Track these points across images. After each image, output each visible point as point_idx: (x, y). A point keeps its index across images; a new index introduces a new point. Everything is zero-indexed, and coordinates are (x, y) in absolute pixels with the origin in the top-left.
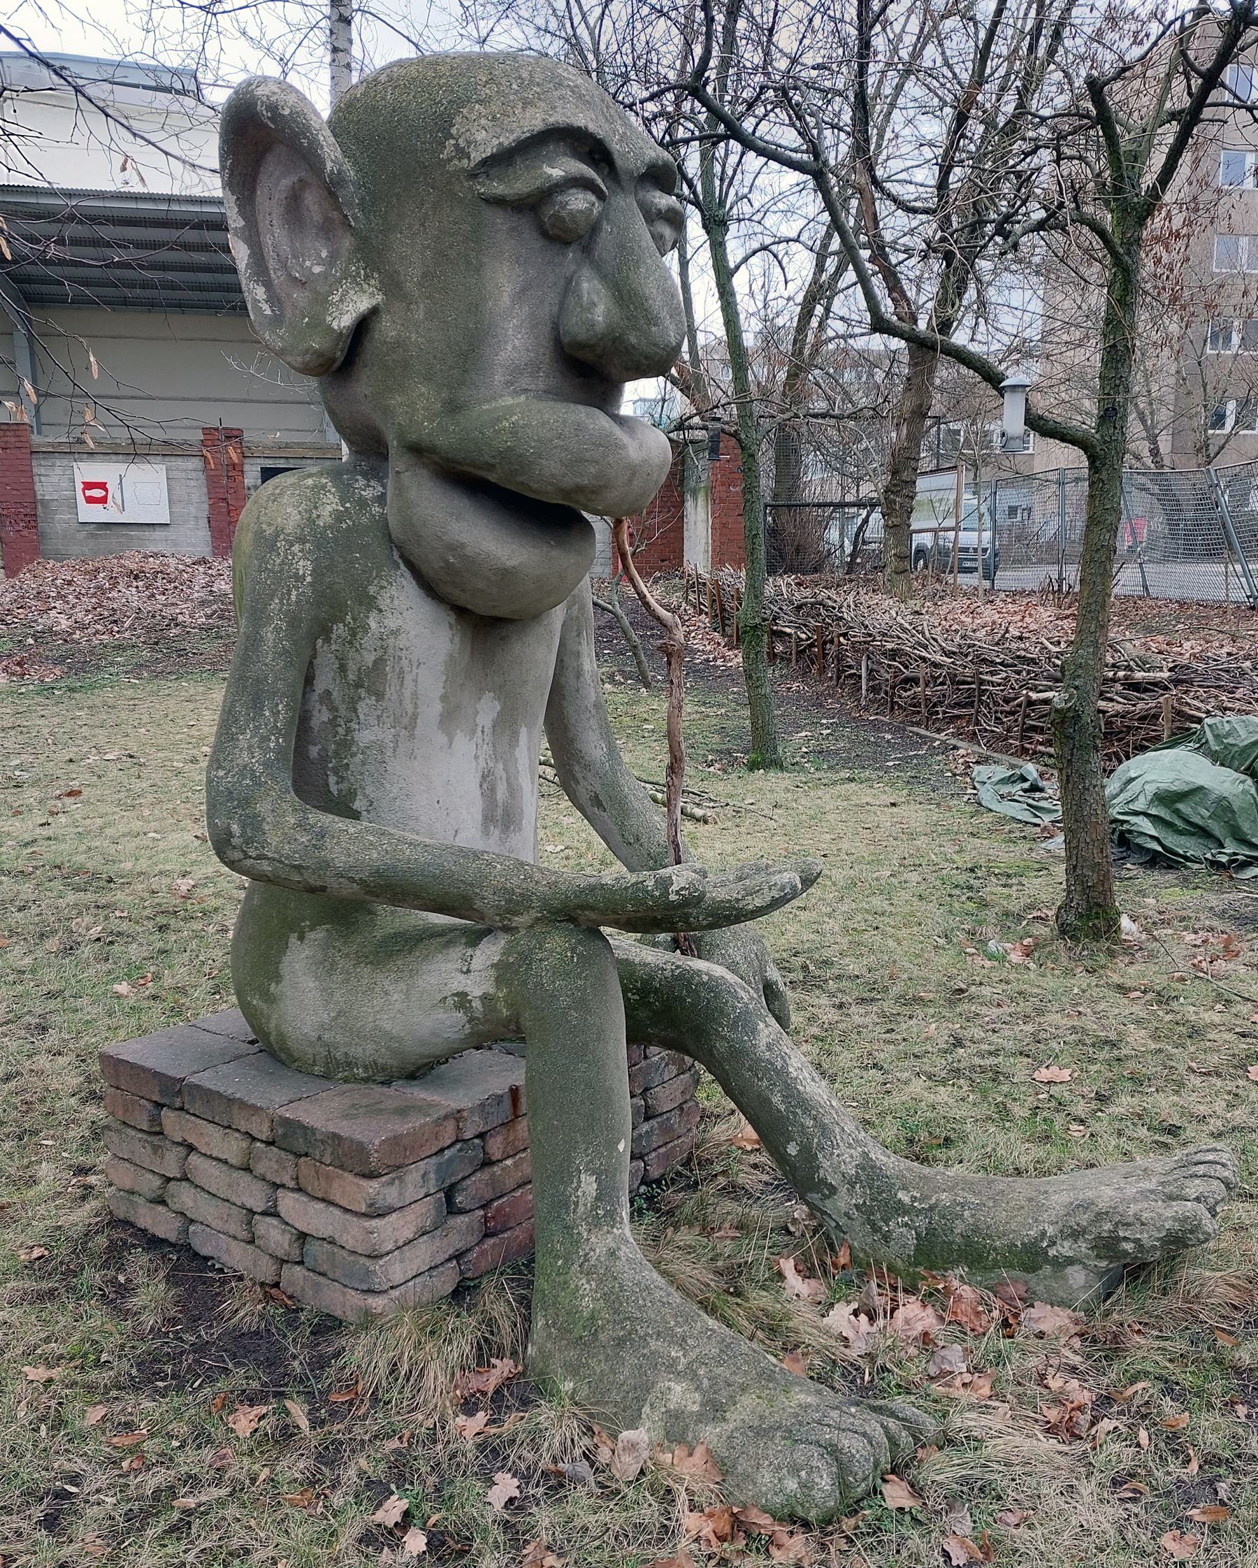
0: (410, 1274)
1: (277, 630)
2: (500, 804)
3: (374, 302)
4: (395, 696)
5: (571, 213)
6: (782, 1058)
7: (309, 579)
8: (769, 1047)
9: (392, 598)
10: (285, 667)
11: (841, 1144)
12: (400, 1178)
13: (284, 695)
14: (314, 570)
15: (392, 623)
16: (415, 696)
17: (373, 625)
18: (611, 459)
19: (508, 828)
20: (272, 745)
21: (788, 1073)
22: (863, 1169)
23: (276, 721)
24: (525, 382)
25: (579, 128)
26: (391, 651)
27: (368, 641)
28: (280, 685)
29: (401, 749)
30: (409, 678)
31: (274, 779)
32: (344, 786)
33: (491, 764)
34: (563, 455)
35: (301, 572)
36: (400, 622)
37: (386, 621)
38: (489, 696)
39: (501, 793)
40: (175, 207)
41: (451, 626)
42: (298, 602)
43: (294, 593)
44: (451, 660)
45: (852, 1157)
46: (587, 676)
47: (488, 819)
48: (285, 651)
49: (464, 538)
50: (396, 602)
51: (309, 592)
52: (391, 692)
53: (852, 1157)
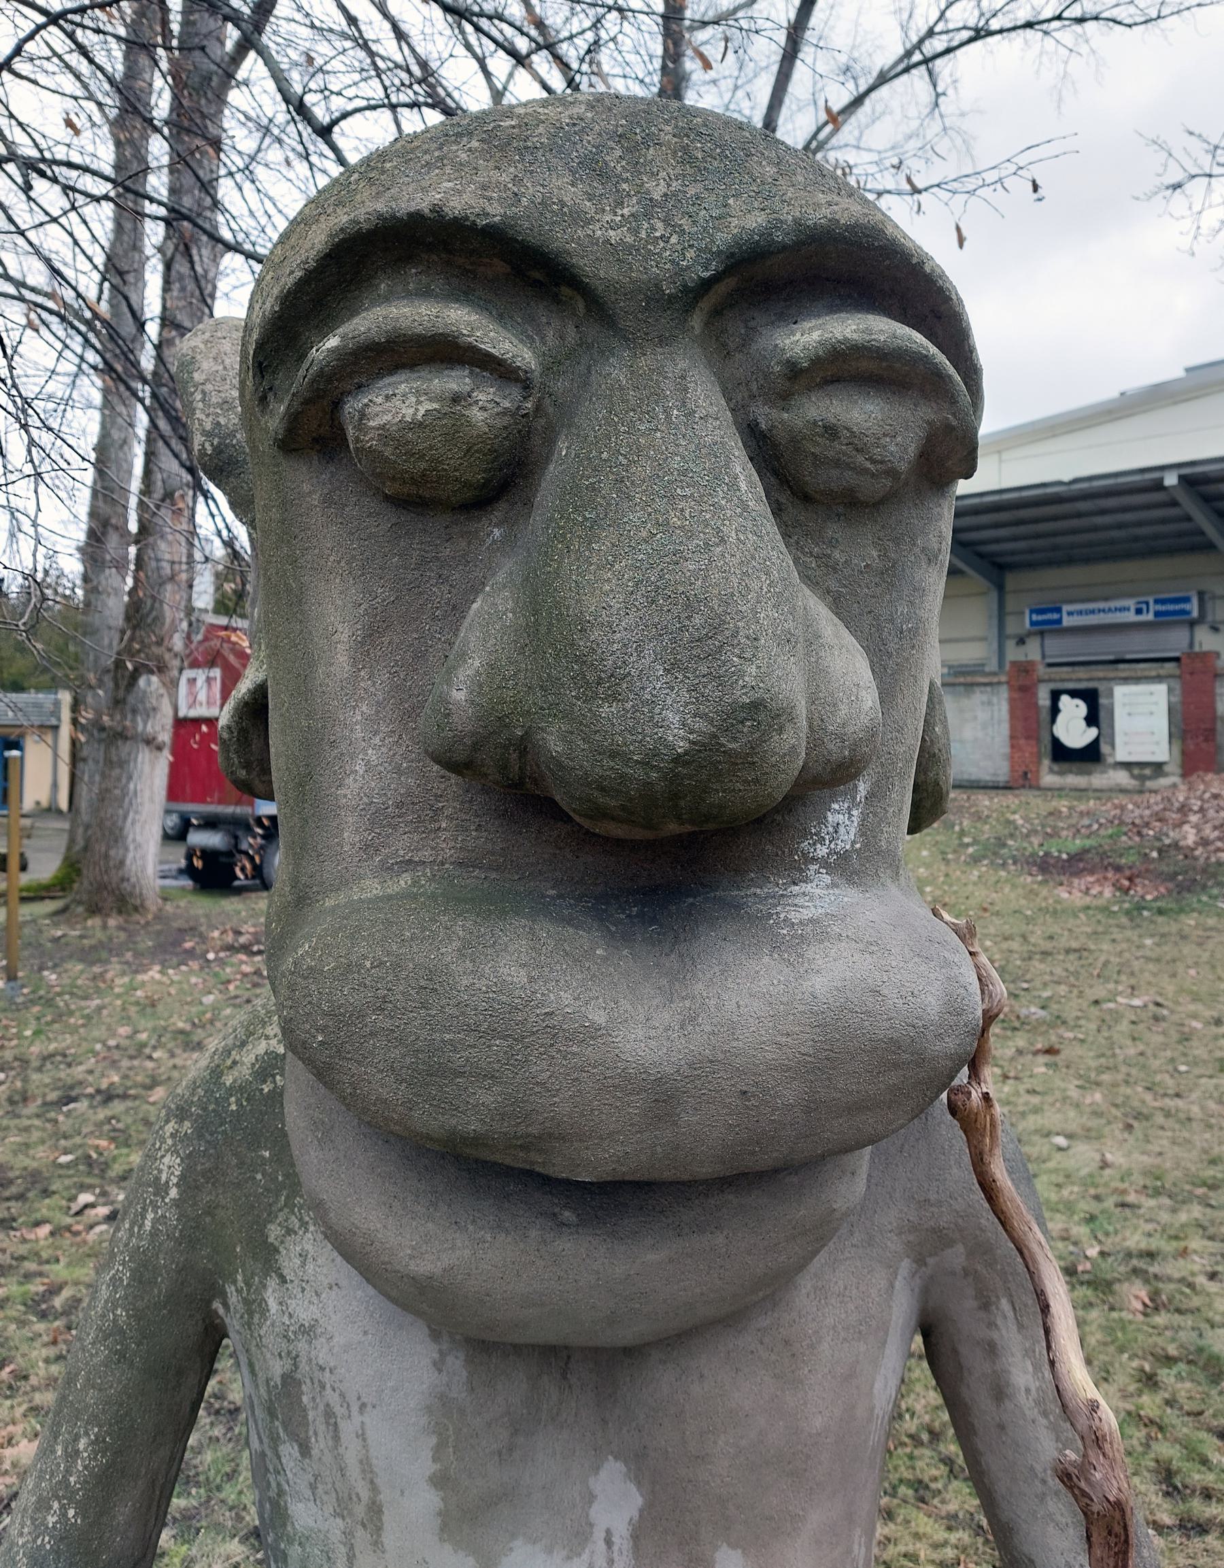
4: (328, 1458)
7: (174, 1193)
13: (94, 1420)
14: (182, 1177)
15: (304, 1310)
16: (366, 1465)
20: (51, 1520)
23: (68, 1472)
24: (401, 844)
25: (416, 218)
26: (304, 1367)
28: (91, 1397)
30: (347, 1429)
34: (396, 1053)
35: (164, 1177)
37: (292, 1303)
42: (154, 1233)
43: (150, 1216)
46: (1022, 1398)
50: (310, 1267)
51: (172, 1216)
52: (320, 1444)
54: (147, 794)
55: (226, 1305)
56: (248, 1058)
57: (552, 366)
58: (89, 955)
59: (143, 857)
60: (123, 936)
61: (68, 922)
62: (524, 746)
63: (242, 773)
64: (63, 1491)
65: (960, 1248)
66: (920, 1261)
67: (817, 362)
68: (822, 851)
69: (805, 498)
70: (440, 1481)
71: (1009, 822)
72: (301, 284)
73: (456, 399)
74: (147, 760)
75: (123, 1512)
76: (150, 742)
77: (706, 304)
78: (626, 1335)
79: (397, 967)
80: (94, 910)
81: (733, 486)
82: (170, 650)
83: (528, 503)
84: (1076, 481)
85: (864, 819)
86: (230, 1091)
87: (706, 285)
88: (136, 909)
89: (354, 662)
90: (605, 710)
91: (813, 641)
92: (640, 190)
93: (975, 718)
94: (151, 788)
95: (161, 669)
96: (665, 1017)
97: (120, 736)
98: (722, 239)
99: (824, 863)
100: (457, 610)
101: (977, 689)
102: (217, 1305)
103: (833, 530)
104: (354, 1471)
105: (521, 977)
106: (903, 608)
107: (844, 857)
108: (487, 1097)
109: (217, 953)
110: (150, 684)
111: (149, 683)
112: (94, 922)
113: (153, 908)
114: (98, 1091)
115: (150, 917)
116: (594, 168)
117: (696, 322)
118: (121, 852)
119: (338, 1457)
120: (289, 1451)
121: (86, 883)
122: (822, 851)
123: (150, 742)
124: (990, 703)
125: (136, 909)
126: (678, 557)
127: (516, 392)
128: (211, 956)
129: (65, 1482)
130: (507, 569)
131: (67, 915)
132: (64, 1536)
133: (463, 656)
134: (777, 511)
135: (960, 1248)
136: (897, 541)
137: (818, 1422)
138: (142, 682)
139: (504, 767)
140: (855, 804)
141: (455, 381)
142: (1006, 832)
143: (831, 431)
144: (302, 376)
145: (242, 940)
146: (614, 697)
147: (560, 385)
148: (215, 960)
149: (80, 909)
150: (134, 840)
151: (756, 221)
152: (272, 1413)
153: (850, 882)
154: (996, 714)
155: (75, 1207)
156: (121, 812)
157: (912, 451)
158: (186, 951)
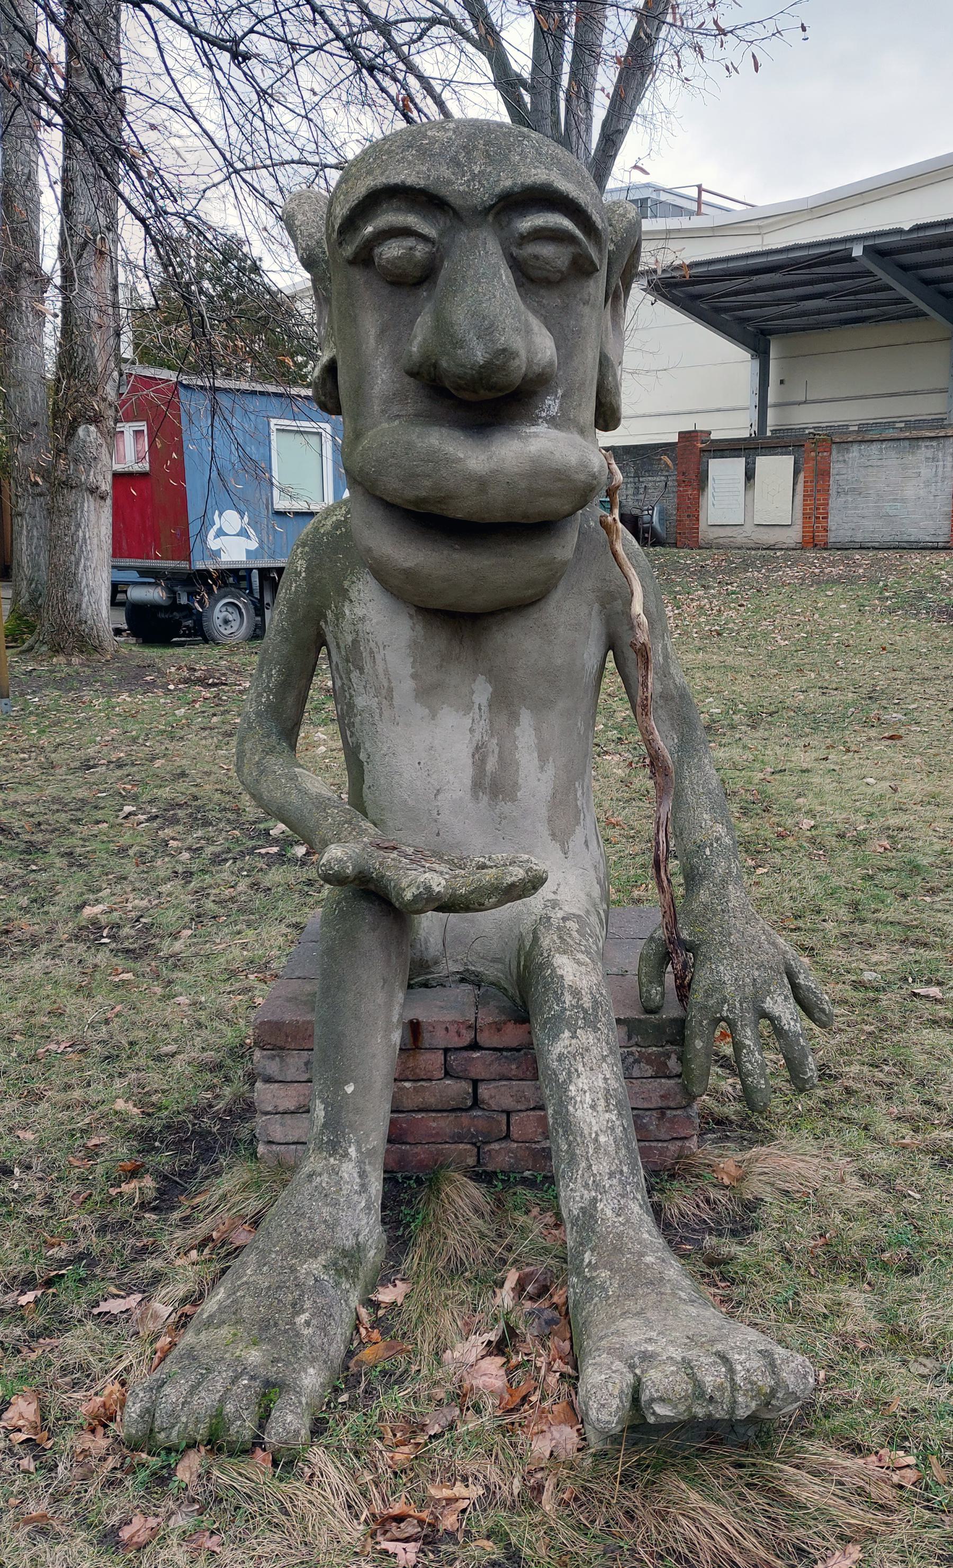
0: (290, 1139)
1: (281, 613)
2: (488, 774)
3: (331, 355)
4: (371, 672)
5: (388, 260)
6: (569, 1073)
7: (303, 574)
8: (560, 1058)
9: (359, 591)
10: (281, 641)
11: (579, 1180)
12: (281, 1057)
13: (278, 663)
15: (360, 611)
16: (386, 672)
17: (347, 612)
18: (444, 473)
19: (496, 796)
21: (567, 1090)
22: (584, 1213)
24: (395, 409)
25: (396, 185)
26: (361, 634)
27: (346, 625)
28: (276, 654)
29: (386, 714)
31: (261, 725)
32: (354, 739)
33: (485, 738)
36: (365, 611)
38: (481, 678)
39: (491, 764)
40: (731, 265)
41: (411, 617)
44: (414, 645)
45: (582, 1197)
47: (477, 785)
48: (283, 629)
49: (372, 544)
52: (368, 668)
53: (582, 1197)
54: (95, 541)
55: (326, 622)
56: (329, 522)
57: (442, 234)
58: (62, 684)
59: (97, 602)
60: (88, 671)
61: (34, 659)
62: (435, 366)
63: (323, 398)
64: (268, 690)
65: (620, 601)
66: (603, 606)
67: (529, 233)
68: (544, 414)
69: (532, 280)
70: (414, 676)
71: (934, 577)
72: (357, 206)
73: (411, 249)
74: (92, 508)
75: (290, 700)
76: (93, 491)
77: (493, 212)
78: (479, 602)
79: (397, 443)
80: (57, 650)
81: (501, 278)
82: (104, 400)
83: (435, 283)
84: (918, 228)
85: (561, 404)
86: (323, 534)
87: (492, 207)
88: (95, 649)
89: (377, 342)
90: (459, 352)
91: (528, 331)
92: (472, 171)
93: (919, 474)
94: (98, 536)
95: (96, 419)
96: (482, 457)
97: (67, 485)
98: (497, 190)
99: (545, 419)
100: (412, 322)
101: (923, 444)
102: (322, 623)
103: (543, 292)
104: (381, 676)
105: (437, 443)
106: (572, 322)
107: (553, 418)
108: (428, 483)
109: (176, 685)
110: (88, 433)
111: (88, 433)
112: (60, 660)
113: (111, 649)
114: (110, 762)
115: (108, 657)
116: (454, 162)
117: (490, 218)
118: (76, 595)
119: (375, 671)
120: (355, 675)
121: (47, 625)
122: (544, 414)
123: (93, 491)
124: (934, 459)
125: (95, 649)
126: (481, 302)
127: (430, 245)
128: (171, 687)
129: (268, 686)
130: (429, 307)
131: (32, 654)
132: (269, 705)
133: (415, 337)
134: (519, 285)
135: (620, 601)
136: (568, 296)
137: (559, 661)
138: (81, 431)
139: (429, 374)
140: (556, 398)
141: (410, 242)
142: (928, 586)
143: (536, 257)
144: (358, 241)
145: (197, 674)
146: (461, 348)
147: (445, 241)
148: (175, 690)
149: (44, 648)
150: (87, 586)
151: (508, 183)
152: (348, 661)
153: (556, 428)
154: (940, 469)
155: (122, 814)
156: (73, 558)
157: (566, 263)
158: (148, 683)
